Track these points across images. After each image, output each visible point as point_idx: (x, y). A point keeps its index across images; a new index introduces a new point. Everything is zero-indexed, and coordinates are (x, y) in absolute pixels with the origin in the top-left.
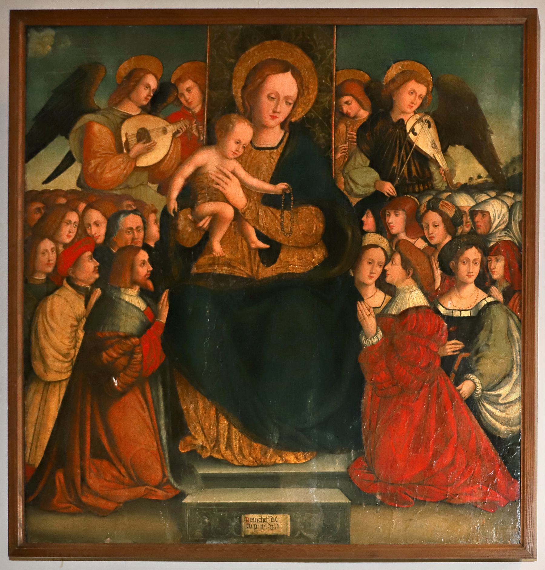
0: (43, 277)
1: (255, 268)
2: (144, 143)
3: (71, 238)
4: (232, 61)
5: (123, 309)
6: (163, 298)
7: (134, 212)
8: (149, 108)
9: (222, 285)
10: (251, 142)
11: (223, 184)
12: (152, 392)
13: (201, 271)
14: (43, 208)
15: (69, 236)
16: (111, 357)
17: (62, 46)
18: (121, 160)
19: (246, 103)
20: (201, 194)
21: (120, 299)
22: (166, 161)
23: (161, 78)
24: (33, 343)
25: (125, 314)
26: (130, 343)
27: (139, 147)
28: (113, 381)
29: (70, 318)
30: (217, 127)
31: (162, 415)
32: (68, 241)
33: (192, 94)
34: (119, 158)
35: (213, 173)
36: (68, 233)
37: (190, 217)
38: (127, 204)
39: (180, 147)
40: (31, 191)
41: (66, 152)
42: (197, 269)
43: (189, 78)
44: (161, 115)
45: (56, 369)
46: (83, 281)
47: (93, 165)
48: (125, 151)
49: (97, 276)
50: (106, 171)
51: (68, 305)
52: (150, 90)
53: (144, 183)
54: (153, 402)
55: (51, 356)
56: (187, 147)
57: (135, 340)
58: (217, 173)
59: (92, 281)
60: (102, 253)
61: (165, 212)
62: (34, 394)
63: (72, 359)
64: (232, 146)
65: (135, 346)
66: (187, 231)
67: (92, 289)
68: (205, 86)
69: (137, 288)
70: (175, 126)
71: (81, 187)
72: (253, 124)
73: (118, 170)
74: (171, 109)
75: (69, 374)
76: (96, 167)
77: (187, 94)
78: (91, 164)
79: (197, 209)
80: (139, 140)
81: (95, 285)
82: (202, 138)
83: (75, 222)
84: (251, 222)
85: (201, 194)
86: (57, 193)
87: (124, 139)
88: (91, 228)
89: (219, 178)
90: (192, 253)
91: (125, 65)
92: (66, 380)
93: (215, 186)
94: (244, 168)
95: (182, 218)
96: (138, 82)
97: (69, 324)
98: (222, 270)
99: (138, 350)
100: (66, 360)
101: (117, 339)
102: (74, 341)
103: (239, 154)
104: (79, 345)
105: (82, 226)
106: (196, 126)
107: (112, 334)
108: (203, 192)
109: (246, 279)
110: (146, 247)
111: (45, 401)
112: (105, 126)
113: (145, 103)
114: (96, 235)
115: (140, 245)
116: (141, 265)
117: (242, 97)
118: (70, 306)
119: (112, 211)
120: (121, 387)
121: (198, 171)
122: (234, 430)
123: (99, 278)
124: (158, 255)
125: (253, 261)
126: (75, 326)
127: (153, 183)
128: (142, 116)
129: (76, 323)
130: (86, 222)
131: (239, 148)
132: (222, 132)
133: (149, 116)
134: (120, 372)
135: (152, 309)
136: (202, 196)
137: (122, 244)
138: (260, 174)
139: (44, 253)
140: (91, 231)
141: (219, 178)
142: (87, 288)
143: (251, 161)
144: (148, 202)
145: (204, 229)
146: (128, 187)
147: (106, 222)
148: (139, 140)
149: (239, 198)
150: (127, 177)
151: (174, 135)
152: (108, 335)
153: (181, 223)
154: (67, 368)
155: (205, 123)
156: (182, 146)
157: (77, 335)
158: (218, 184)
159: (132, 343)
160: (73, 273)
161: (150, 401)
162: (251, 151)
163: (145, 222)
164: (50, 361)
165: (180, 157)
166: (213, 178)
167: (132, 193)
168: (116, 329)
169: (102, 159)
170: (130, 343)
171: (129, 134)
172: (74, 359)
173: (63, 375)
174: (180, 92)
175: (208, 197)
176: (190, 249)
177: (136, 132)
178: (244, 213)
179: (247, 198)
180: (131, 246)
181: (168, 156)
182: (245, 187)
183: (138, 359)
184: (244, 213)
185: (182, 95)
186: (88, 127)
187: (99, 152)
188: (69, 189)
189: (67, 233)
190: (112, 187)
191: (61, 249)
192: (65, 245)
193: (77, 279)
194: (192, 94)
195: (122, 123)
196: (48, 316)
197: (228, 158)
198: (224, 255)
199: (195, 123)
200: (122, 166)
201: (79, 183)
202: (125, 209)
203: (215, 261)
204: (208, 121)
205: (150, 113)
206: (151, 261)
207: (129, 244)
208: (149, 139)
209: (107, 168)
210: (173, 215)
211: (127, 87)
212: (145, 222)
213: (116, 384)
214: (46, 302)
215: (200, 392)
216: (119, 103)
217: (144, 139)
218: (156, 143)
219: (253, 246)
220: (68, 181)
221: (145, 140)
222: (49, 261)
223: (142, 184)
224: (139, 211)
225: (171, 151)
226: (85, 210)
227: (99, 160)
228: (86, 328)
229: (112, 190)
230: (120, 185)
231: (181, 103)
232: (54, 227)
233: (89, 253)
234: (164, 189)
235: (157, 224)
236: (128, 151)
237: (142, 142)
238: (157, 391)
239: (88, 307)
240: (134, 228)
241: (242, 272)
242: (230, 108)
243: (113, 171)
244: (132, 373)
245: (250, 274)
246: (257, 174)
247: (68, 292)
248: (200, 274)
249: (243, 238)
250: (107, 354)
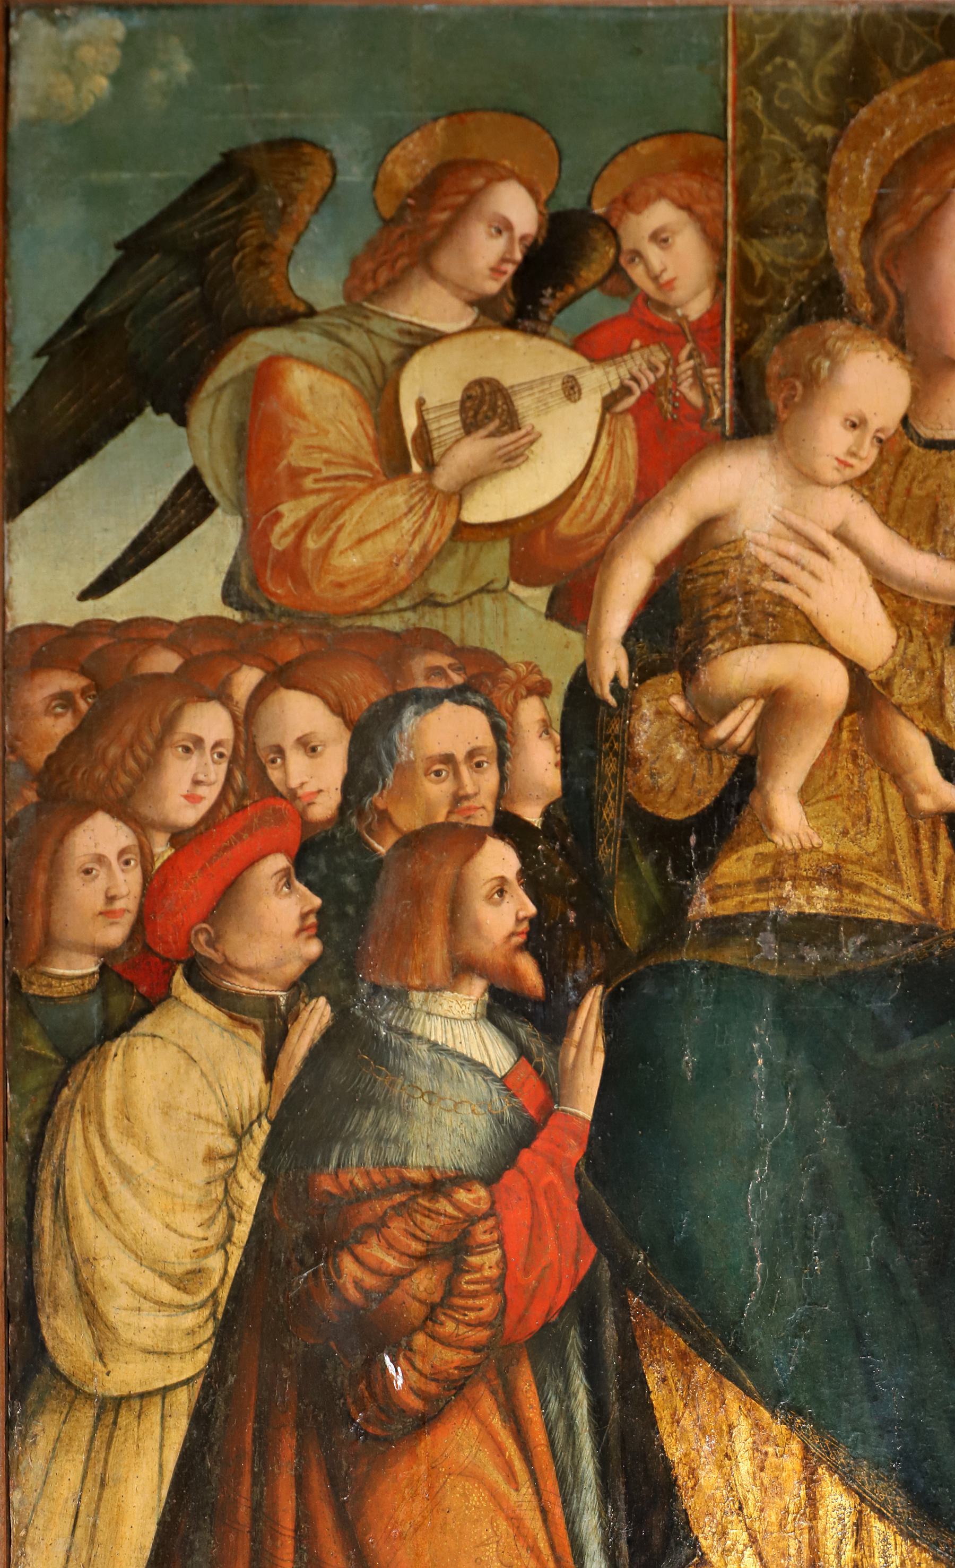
0: (88, 966)
1: (936, 885)
2: (491, 435)
3: (203, 807)
4: (827, 131)
5: (423, 1077)
6: (580, 1023)
7: (459, 695)
8: (509, 309)
9: (813, 955)
10: (905, 421)
11: (804, 578)
12: (544, 1404)
13: (728, 907)
14: (84, 693)
15: (192, 798)
16: (376, 1272)
17: (157, 76)
18: (400, 499)
19: (881, 280)
20: (718, 617)
21: (408, 1035)
22: (578, 500)
23: (552, 196)
24: (47, 1240)
25: (431, 1093)
26: (450, 1210)
27: (473, 450)
28: (385, 1369)
29: (201, 1126)
30: (774, 369)
31: (589, 1497)
32: (189, 816)
33: (672, 252)
34: (392, 493)
35: (764, 539)
36: (187, 787)
37: (678, 704)
38: (422, 668)
39: (631, 447)
40: (30, 628)
41: (179, 475)
42: (713, 900)
43: (661, 195)
44: (553, 332)
45: (145, 1340)
46: (249, 972)
47: (286, 522)
48: (416, 468)
49: (314, 948)
50: (343, 541)
51: (195, 1074)
52: (511, 240)
53: (497, 586)
54: (552, 1443)
55: (123, 1289)
56: (665, 444)
57: (473, 1197)
58: (779, 537)
59: (294, 969)
60: (333, 859)
61: (581, 688)
62: (53, 1456)
63: (214, 1294)
64: (832, 440)
65: (472, 1219)
66: (670, 758)
67: (290, 1005)
68: (725, 223)
69: (477, 988)
70: (612, 370)
71: (240, 607)
72: (909, 358)
73: (390, 540)
74: (595, 307)
75: (203, 1356)
76: (302, 530)
77: (654, 254)
78: (278, 517)
79: (704, 677)
80: (470, 427)
81: (306, 983)
82: (717, 412)
83: (217, 744)
84: (918, 715)
85: (718, 617)
86: (142, 632)
87: (410, 423)
88: (284, 764)
89: (787, 557)
90: (693, 840)
91: (413, 146)
92: (187, 1382)
93: (770, 585)
94: (884, 517)
95: (647, 710)
96: (461, 213)
97: (201, 1150)
98: (809, 899)
99: (482, 1233)
100: (187, 1299)
101: (398, 1198)
102: (222, 1218)
103: (861, 467)
104: (242, 1231)
105: (249, 758)
106: (694, 369)
107: (377, 1178)
108: (727, 609)
109: (906, 928)
110: (507, 826)
111: (100, 1480)
112: (336, 375)
113: (492, 287)
114: (308, 789)
115: (485, 819)
116: (489, 898)
117: (866, 263)
118: (203, 1074)
119: (368, 690)
120: (419, 1394)
121: (704, 533)
122: (877, 1527)
123: (321, 958)
124: (560, 853)
125: (927, 860)
126: (223, 1158)
127: (530, 582)
128: (482, 336)
129: (229, 1145)
130: (264, 740)
131: (860, 445)
132: (794, 388)
133: (509, 335)
134: (414, 1330)
135: (537, 1069)
136: (722, 625)
137: (408, 819)
138: (941, 537)
139: (88, 872)
140: (286, 773)
141: (787, 557)
142: (272, 999)
143: (908, 491)
144: (513, 656)
145: (735, 750)
146: (430, 601)
147: (347, 736)
148: (470, 427)
149: (872, 635)
150: (426, 563)
151: (609, 403)
152: (360, 1182)
153: (645, 730)
154: (191, 1332)
155: (728, 356)
156: (641, 439)
157: (235, 1192)
158: (784, 580)
159: (457, 1206)
160: (211, 943)
161: (538, 1436)
162: (908, 451)
163: (503, 732)
164: (117, 1308)
165: (632, 484)
166: (766, 557)
167: (450, 624)
168: (392, 1154)
169: (326, 497)
170: (450, 1210)
171: (431, 402)
172: (224, 1294)
173: (176, 1364)
174: (627, 245)
175: (745, 630)
176: (680, 829)
177: (458, 397)
178: (887, 684)
179: (897, 628)
180: (449, 828)
181: (588, 483)
182: (884, 584)
183: (487, 1273)
184: (887, 684)
185: (637, 254)
186: (264, 379)
187: (310, 471)
188: (189, 615)
189: (185, 786)
190: (367, 603)
191: (162, 849)
192: (178, 837)
193: (229, 967)
194: (672, 252)
195: (402, 362)
196: (109, 1123)
197: (818, 483)
198: (816, 841)
199: (690, 357)
200: (407, 525)
201: (231, 593)
202: (421, 683)
203: (780, 869)
204: (741, 347)
205: (511, 325)
206: (531, 880)
207: (441, 818)
208: (511, 422)
209: (348, 528)
210: (612, 701)
211: (414, 232)
212: (503, 732)
213: (399, 1382)
214: (100, 1067)
215: (738, 1382)
216: (394, 285)
217: (490, 419)
218: (540, 435)
219: (925, 803)
220: (190, 583)
221: (492, 426)
222: (111, 899)
223: (484, 590)
224: (476, 692)
225: (597, 464)
226: (260, 694)
227: (312, 502)
228: (267, 1162)
229: (367, 612)
230: (401, 594)
231: (633, 286)
232: (131, 763)
233: (279, 862)
234: (574, 604)
235: (551, 737)
236: (430, 466)
237: (483, 432)
238: (566, 1395)
239: (277, 1076)
240: (460, 755)
241: (888, 905)
242: (824, 299)
243: (368, 545)
244: (462, 1330)
245: (917, 907)
246: (932, 535)
247: (190, 1019)
248: (727, 918)
249: (887, 777)
250: (357, 1259)
